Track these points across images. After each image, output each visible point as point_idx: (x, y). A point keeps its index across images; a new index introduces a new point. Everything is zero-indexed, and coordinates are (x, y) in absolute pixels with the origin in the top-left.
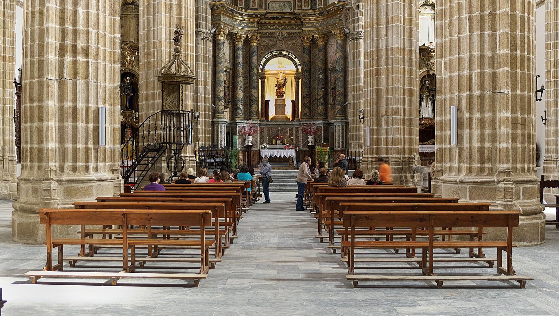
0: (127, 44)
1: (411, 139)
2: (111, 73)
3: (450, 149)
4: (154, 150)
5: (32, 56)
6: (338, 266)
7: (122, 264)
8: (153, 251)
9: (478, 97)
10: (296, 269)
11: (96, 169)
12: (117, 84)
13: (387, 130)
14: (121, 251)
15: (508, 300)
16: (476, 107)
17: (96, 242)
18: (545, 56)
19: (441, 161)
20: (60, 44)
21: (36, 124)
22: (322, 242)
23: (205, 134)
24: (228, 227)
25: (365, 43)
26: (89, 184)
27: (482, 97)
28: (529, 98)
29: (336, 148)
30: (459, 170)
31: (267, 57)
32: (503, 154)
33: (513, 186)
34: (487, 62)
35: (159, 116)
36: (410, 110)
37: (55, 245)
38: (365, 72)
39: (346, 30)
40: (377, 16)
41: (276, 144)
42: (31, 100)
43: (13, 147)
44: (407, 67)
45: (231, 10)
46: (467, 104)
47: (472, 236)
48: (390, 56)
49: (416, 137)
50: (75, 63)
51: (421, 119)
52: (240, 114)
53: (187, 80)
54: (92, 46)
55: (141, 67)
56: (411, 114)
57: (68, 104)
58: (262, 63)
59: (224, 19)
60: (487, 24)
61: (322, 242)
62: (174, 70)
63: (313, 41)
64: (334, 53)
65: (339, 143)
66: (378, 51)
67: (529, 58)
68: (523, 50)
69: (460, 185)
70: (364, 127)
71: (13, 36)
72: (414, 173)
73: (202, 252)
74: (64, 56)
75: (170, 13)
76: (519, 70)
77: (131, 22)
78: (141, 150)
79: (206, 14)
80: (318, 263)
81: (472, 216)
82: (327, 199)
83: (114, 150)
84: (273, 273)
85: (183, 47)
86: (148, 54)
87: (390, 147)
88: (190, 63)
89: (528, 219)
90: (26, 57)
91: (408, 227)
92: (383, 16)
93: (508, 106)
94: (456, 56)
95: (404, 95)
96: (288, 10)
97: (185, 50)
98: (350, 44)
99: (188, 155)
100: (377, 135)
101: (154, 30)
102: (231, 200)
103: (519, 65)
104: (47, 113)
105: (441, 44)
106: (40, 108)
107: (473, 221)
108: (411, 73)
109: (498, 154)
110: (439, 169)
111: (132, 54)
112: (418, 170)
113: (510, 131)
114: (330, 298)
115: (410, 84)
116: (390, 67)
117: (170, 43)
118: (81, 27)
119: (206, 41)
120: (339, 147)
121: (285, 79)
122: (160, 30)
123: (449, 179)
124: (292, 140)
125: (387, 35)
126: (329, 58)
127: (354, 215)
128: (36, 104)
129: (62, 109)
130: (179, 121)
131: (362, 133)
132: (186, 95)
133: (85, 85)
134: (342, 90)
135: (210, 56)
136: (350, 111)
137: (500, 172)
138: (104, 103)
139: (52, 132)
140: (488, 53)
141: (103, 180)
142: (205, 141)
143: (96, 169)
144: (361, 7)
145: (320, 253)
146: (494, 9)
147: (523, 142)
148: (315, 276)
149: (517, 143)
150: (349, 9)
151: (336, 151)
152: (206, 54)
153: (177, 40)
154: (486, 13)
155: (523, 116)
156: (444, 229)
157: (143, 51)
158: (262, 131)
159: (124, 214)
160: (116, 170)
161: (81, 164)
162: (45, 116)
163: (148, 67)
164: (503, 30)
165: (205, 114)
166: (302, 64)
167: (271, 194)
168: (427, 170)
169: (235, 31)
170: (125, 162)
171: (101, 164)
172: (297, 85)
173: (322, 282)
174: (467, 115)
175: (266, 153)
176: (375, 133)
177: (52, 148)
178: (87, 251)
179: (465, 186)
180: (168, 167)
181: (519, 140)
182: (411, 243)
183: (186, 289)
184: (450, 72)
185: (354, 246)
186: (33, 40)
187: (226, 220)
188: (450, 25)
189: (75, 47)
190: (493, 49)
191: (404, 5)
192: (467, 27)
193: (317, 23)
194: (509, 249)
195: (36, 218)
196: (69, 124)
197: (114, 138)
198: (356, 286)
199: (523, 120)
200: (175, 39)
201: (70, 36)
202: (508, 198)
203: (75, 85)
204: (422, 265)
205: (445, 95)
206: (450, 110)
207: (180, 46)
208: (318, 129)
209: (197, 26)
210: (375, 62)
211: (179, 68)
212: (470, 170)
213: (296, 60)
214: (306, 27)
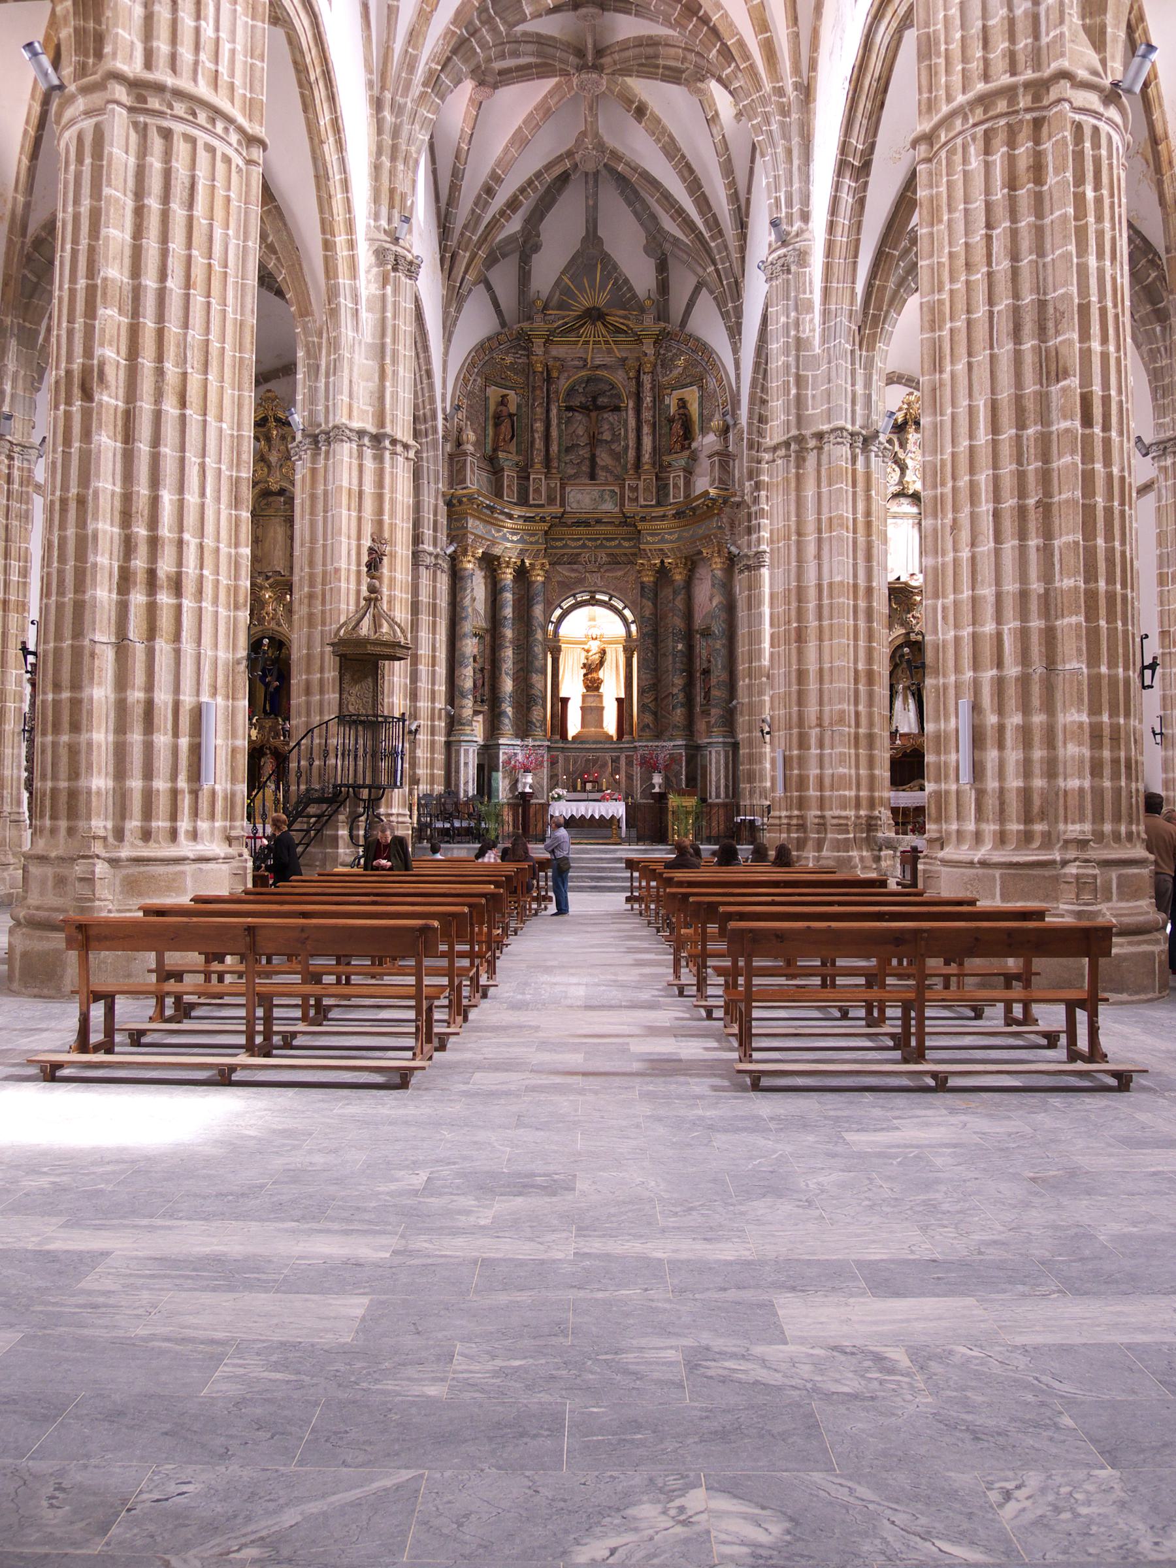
0: (268, 578)
1: (872, 778)
2: (228, 629)
3: (958, 792)
4: (319, 801)
5: (61, 592)
6: (715, 1045)
7: (242, 1040)
8: (312, 1012)
9: (1017, 679)
10: (624, 1050)
11: (194, 835)
12: (242, 653)
13: (821, 757)
14: (242, 1013)
15: (1093, 1117)
16: (1012, 702)
17: (190, 989)
18: (1156, 600)
19: (938, 820)
20: (121, 568)
21: (65, 738)
22: (681, 994)
23: (432, 767)
24: (477, 961)
25: (771, 578)
26: (179, 868)
27: (1024, 681)
28: (1127, 682)
29: (713, 800)
30: (978, 837)
31: (565, 605)
32: (1073, 802)
33: (1097, 871)
34: (1034, 606)
35: (333, 727)
36: (870, 716)
37: (97, 996)
38: (772, 636)
39: (733, 549)
40: (798, 515)
41: (584, 790)
42: (57, 687)
43: (19, 793)
44: (862, 624)
45: (488, 507)
46: (992, 695)
47: (1009, 979)
48: (826, 601)
49: (883, 773)
50: (152, 609)
51: (894, 735)
52: (507, 725)
53: (394, 651)
54: (190, 571)
55: (296, 624)
56: (871, 724)
57: (136, 695)
58: (554, 619)
59: (474, 525)
60: (1032, 526)
61: (681, 994)
62: (365, 629)
63: (662, 573)
64: (706, 597)
65: (718, 788)
66: (800, 591)
67: (1124, 598)
68: (1110, 580)
69: (980, 871)
70: (773, 750)
71: (25, 557)
72: (880, 850)
73: (419, 1013)
74: (128, 593)
75: (360, 511)
76: (1103, 623)
77: (277, 531)
78: (293, 799)
79: (435, 514)
80: (672, 1040)
81: (1010, 932)
82: (691, 899)
83: (233, 794)
84: (575, 1060)
85: (386, 581)
86: (311, 596)
87: (827, 793)
88: (401, 614)
89: (1130, 943)
90: (48, 595)
91: (867, 957)
92: (810, 517)
93: (1081, 700)
94: (966, 594)
95: (856, 681)
96: (609, 506)
97: (390, 588)
98: (740, 579)
99: (394, 811)
100: (800, 768)
101: (325, 546)
102: (483, 901)
103: (1103, 611)
104: (90, 713)
105: (935, 569)
106: (76, 703)
107: (1010, 943)
108: (870, 637)
109: (1061, 801)
110: (935, 835)
111: (280, 599)
112: (890, 845)
113: (1086, 752)
114: (700, 1112)
115: (870, 660)
116: (826, 623)
117: (359, 572)
118: (166, 531)
119: (435, 573)
120: (718, 796)
121: (603, 653)
122: (336, 545)
123: (955, 857)
124: (618, 782)
125: (819, 557)
126: (696, 608)
127: (751, 931)
128: (66, 695)
129: (121, 707)
130: (375, 739)
131: (768, 766)
132: (391, 683)
133: (172, 655)
134: (724, 676)
135: (443, 603)
136: (742, 720)
137: (1066, 842)
138: (214, 694)
139: (99, 755)
140: (1036, 587)
141: (207, 860)
142: (432, 783)
143: (194, 835)
144: (763, 499)
145: (677, 1019)
146: (1048, 494)
147: (1116, 776)
148: (666, 1066)
149: (1102, 777)
150: (738, 505)
151: (711, 805)
152: (435, 598)
153: (374, 565)
154: (1031, 501)
155: (1114, 720)
156: (947, 963)
157: (301, 591)
158: (553, 763)
159: (251, 930)
160: (237, 838)
161: (160, 824)
162: (84, 722)
163: (311, 624)
164: (1068, 537)
165: (433, 727)
166: (640, 620)
167: (572, 897)
168: (910, 840)
169: (497, 551)
170: (260, 827)
171: (203, 825)
172: (629, 665)
173: (682, 1079)
174: (992, 719)
175: (562, 809)
176: (795, 765)
177: (99, 789)
178: (169, 1012)
179: (990, 871)
180: (351, 836)
181: (1107, 771)
182: (875, 994)
183: (382, 1092)
184: (956, 627)
185: (749, 997)
186: (62, 559)
187: (472, 948)
188: (953, 528)
189: (152, 573)
190: (1047, 577)
191: (854, 493)
192: (991, 532)
193: (670, 534)
194: (1091, 1004)
195: (57, 940)
196: (136, 737)
197: (233, 769)
198: (756, 1087)
199: (1116, 729)
200: (369, 565)
201: (142, 550)
202: (1086, 897)
203: (150, 654)
204: (901, 1042)
205: (944, 676)
206: (957, 709)
207: (380, 579)
208: (673, 759)
209: (417, 539)
210: (793, 614)
211: (376, 625)
212: (1002, 839)
213: (627, 612)
214: (648, 543)
